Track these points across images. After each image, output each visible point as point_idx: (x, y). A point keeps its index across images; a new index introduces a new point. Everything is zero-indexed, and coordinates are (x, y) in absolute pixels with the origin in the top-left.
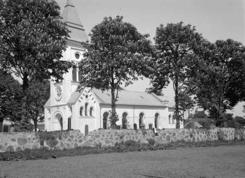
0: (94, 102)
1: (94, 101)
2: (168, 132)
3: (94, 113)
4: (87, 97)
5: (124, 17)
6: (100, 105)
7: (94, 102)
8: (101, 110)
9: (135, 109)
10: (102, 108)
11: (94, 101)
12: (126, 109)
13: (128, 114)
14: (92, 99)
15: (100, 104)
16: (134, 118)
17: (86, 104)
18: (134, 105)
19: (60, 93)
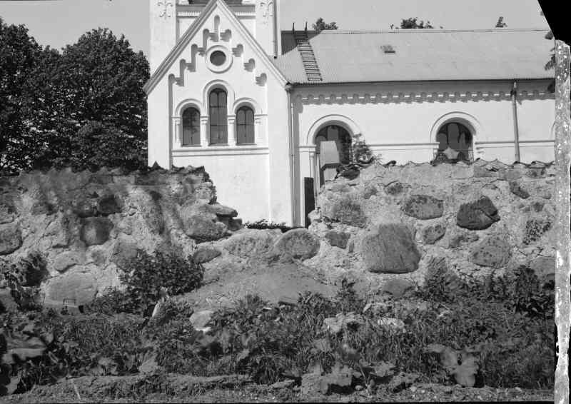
0: (261, 80)
1: (256, 72)
2: (395, 189)
3: (261, 129)
4: (218, 57)
5: (336, 21)
6: (289, 91)
7: (261, 80)
8: (305, 26)
9: (526, 102)
10: (304, 30)
11: (256, 72)
12: (459, 102)
13: (474, 130)
14: (249, 65)
15: (288, 84)
16: (518, 148)
17: (218, 93)
18: (512, 81)
19: (481, 298)
